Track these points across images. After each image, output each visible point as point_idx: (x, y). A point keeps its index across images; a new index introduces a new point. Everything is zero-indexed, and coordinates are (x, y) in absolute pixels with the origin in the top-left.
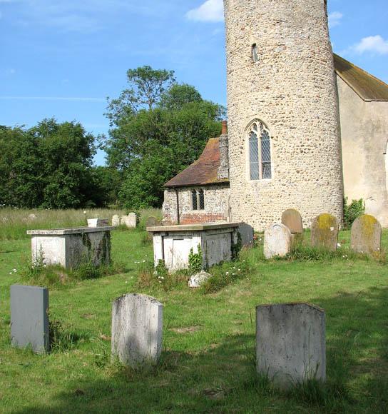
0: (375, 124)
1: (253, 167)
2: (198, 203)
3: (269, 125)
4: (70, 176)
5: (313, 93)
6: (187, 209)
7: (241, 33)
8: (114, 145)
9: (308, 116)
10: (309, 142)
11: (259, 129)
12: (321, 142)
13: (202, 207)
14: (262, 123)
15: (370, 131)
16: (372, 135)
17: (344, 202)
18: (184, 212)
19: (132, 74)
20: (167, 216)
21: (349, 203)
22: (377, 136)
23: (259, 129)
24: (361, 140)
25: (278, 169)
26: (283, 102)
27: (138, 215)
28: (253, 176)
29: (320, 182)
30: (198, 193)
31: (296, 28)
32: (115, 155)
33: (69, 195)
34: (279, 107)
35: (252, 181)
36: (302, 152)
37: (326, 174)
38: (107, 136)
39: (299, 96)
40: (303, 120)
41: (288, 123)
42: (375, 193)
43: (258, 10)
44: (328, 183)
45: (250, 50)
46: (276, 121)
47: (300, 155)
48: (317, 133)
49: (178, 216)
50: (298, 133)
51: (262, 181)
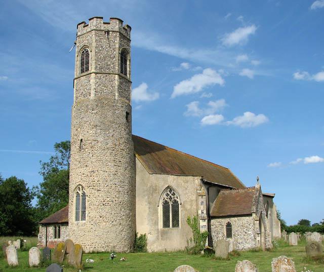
0: (154, 188)
1: (77, 213)
2: (57, 234)
3: (86, 188)
4: (6, 214)
5: (113, 170)
6: (51, 239)
7: (76, 132)
8: (44, 194)
9: (109, 183)
10: (108, 199)
11: (81, 191)
12: (117, 199)
13: (59, 237)
14: (82, 187)
15: (151, 192)
16: (152, 195)
17: (136, 235)
18: (50, 240)
19: (57, 146)
20: (40, 242)
21: (139, 236)
22: (155, 195)
23: (81, 191)
24: (147, 197)
25: (89, 215)
26: (95, 175)
27: (22, 241)
28: (77, 219)
29: (114, 223)
30: (57, 228)
31: (105, 130)
32: (43, 202)
33: (5, 227)
34: (92, 178)
35: (86, 219)
36: (104, 205)
37: (119, 218)
38: (39, 186)
39: (104, 171)
40: (106, 186)
41: (96, 188)
42: (153, 230)
43: (85, 119)
44: (120, 224)
45: (79, 143)
46: (90, 186)
47: (103, 207)
48: (114, 194)
49: (47, 242)
50: (102, 194)
51: (81, 222)
